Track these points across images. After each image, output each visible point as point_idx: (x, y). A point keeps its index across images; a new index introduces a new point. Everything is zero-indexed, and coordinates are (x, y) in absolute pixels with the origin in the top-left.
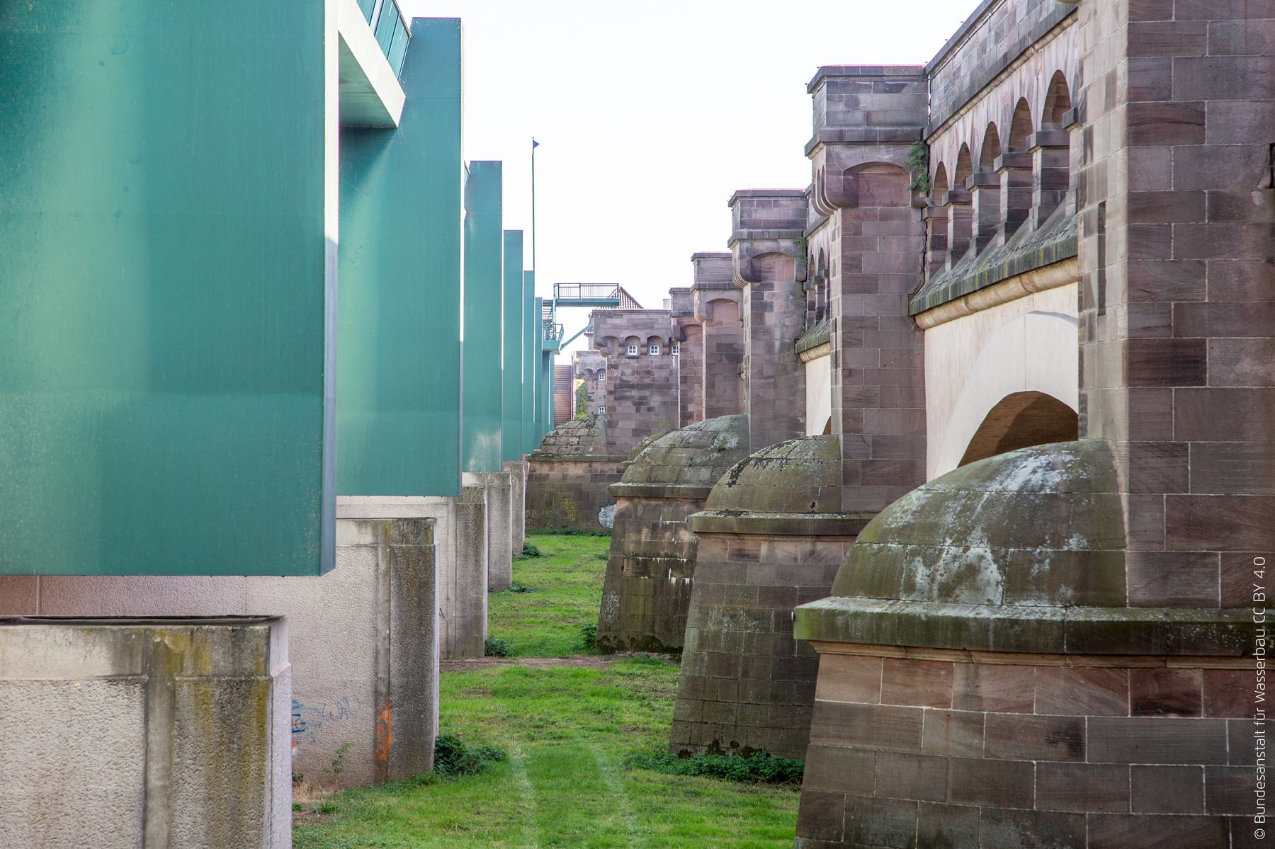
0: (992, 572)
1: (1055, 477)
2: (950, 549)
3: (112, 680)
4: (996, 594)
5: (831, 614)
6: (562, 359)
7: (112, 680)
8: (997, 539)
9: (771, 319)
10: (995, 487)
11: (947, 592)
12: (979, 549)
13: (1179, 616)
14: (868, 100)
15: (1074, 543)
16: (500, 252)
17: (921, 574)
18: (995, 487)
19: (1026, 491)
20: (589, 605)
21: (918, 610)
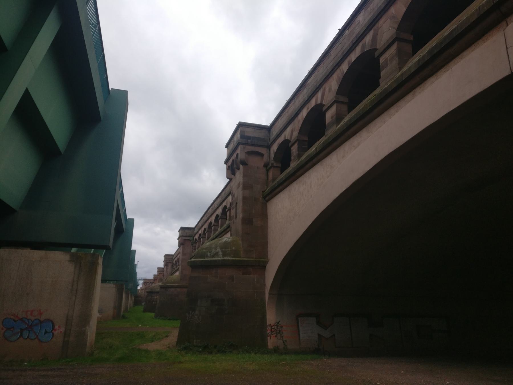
0: (220, 253)
1: (230, 240)
2: (214, 250)
3: (69, 261)
4: (221, 256)
5: (194, 261)
6: (139, 288)
7: (69, 261)
8: (221, 248)
9: (168, 270)
10: (220, 241)
11: (213, 257)
12: (218, 250)
13: (249, 259)
14: (186, 231)
15: (233, 248)
16: (133, 267)
17: (209, 254)
18: (220, 241)
19: (226, 242)
20: (142, 310)
21: (209, 259)
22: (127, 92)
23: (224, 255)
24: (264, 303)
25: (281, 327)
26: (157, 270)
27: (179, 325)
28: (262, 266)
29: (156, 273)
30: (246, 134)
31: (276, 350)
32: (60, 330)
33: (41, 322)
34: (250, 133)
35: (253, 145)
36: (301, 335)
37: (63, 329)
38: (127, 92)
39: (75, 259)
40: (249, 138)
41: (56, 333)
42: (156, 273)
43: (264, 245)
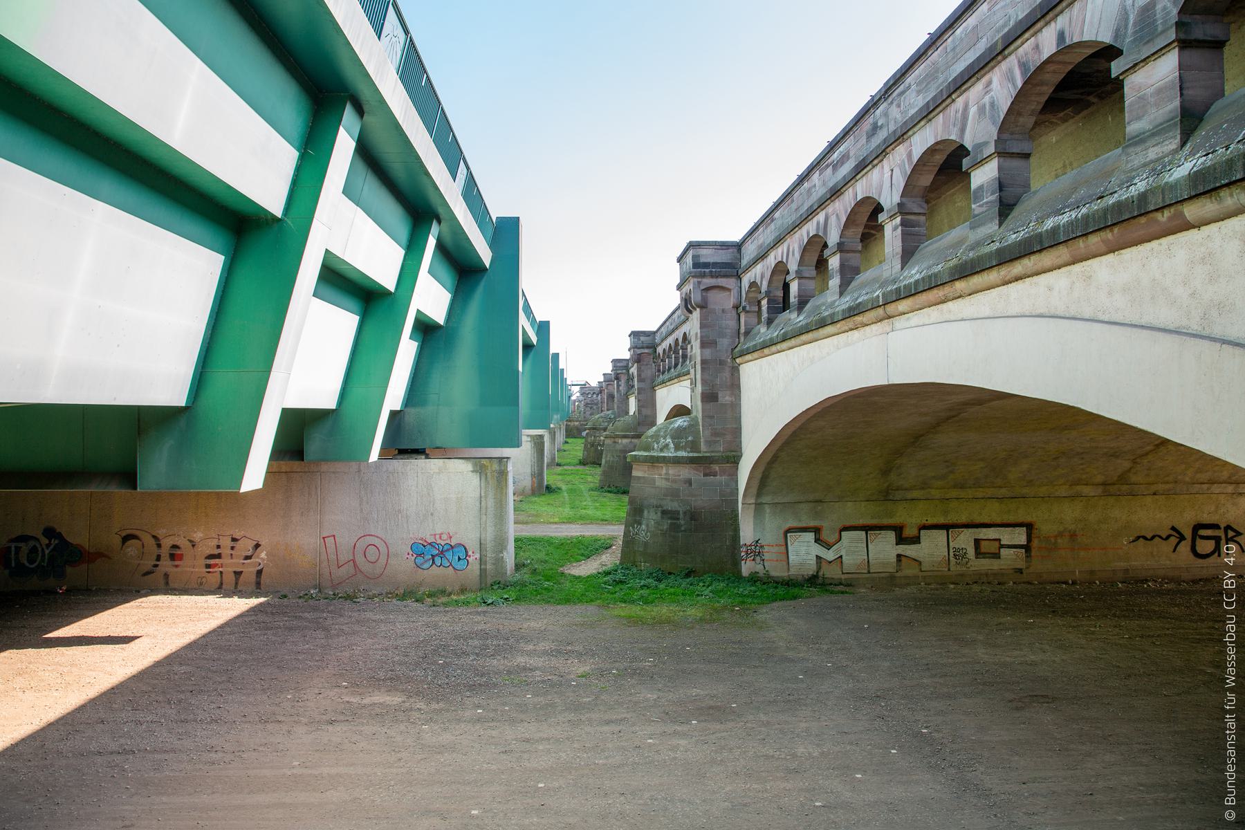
8: (673, 438)
11: (661, 450)
12: (669, 440)
14: (642, 338)
22: (284, 410)
23: (677, 448)
24: (737, 515)
25: (762, 547)
26: (627, 343)
27: (623, 514)
28: (733, 459)
29: (626, 355)
30: (702, 260)
31: (754, 579)
32: (474, 557)
33: (452, 547)
34: (708, 256)
35: (712, 276)
36: (791, 558)
37: (478, 556)
38: (284, 410)
39: (480, 467)
40: (706, 265)
41: (470, 560)
42: (626, 355)
43: (737, 432)
